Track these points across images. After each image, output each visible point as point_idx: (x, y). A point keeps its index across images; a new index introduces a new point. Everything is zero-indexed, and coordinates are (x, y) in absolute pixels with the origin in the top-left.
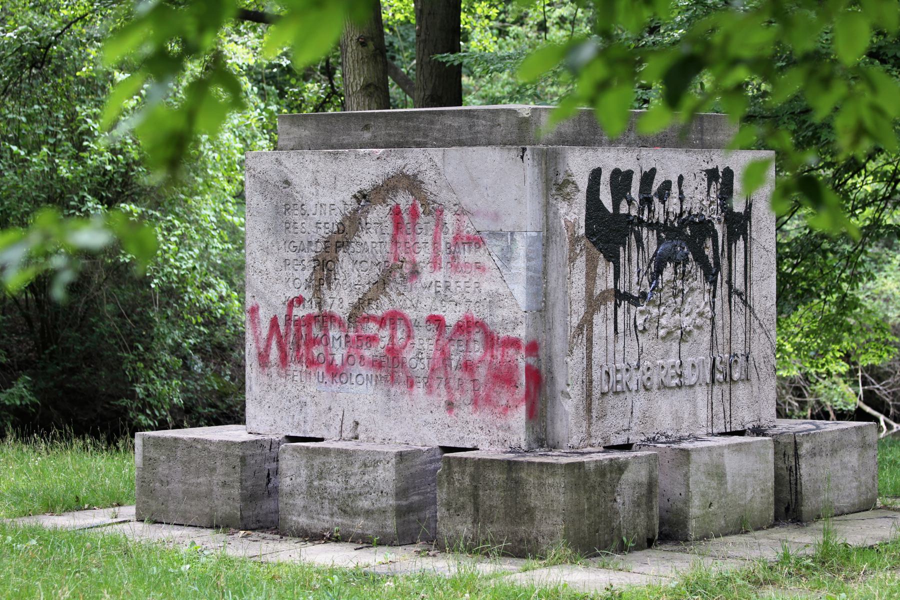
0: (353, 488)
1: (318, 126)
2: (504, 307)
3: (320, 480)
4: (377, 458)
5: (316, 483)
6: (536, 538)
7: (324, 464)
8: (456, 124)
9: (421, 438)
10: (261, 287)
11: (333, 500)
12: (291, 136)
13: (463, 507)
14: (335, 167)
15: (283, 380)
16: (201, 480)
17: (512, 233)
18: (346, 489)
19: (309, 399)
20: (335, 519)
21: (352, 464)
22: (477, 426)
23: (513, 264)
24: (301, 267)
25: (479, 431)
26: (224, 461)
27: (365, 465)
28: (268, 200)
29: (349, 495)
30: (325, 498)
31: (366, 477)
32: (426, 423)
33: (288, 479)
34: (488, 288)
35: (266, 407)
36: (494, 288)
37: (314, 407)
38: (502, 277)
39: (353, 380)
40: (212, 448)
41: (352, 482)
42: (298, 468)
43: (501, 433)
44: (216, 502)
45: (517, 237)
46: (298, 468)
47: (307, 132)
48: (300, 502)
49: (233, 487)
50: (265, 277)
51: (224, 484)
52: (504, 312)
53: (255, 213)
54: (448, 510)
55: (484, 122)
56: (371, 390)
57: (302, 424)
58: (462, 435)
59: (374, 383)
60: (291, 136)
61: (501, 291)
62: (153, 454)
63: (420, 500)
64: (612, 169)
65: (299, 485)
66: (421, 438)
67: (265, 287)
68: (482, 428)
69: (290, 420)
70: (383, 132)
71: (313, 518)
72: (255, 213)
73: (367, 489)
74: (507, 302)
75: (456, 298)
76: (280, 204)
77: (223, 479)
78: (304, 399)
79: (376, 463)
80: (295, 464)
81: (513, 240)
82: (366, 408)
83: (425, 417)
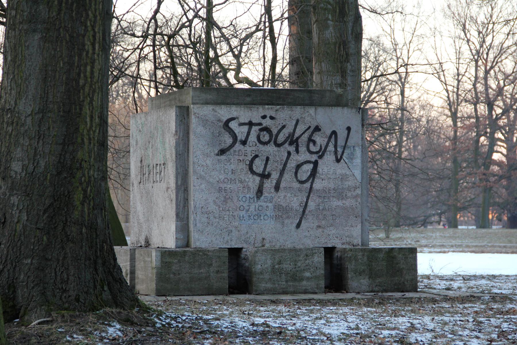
0: (299, 267)
1: (218, 93)
2: (349, 180)
3: (280, 264)
4: (314, 251)
5: (276, 267)
6: (404, 283)
7: (282, 257)
8: (302, 96)
9: (302, 244)
10: (202, 173)
11: (287, 274)
12: (201, 98)
13: (364, 271)
14: (250, 114)
15: (217, 220)
16: (202, 271)
17: (354, 147)
18: (295, 268)
19: (234, 229)
20: (289, 283)
21: (299, 256)
22: (334, 236)
23: (354, 161)
24: (229, 163)
25: (336, 239)
26: (218, 260)
27: (307, 256)
28: (208, 129)
29: (297, 271)
30: (282, 273)
31: (307, 262)
32: (306, 236)
33: (259, 266)
34: (341, 172)
35: (206, 234)
36: (344, 172)
37: (237, 233)
38: (348, 167)
39: (262, 218)
40: (210, 254)
41: (299, 264)
42: (266, 259)
43: (348, 239)
44: (212, 281)
45: (357, 148)
46: (266, 259)
47: (211, 97)
48: (267, 276)
49: (224, 273)
50: (206, 168)
51: (218, 272)
52: (350, 183)
53: (199, 136)
54: (355, 273)
55: (317, 96)
56: (273, 222)
57: (230, 241)
58: (326, 241)
59: (274, 219)
60: (201, 98)
61: (348, 173)
62: (168, 260)
63: (127, 283)
64: (270, 120)
65: (267, 268)
66: (302, 244)
67: (206, 174)
68: (337, 237)
69: (222, 240)
70: (259, 98)
71: (275, 284)
72: (199, 136)
73: (308, 267)
74: (351, 178)
75: (322, 177)
76: (215, 132)
77: (216, 269)
78: (231, 229)
79: (313, 254)
80: (264, 258)
81: (354, 150)
82: (269, 231)
83: (304, 234)
